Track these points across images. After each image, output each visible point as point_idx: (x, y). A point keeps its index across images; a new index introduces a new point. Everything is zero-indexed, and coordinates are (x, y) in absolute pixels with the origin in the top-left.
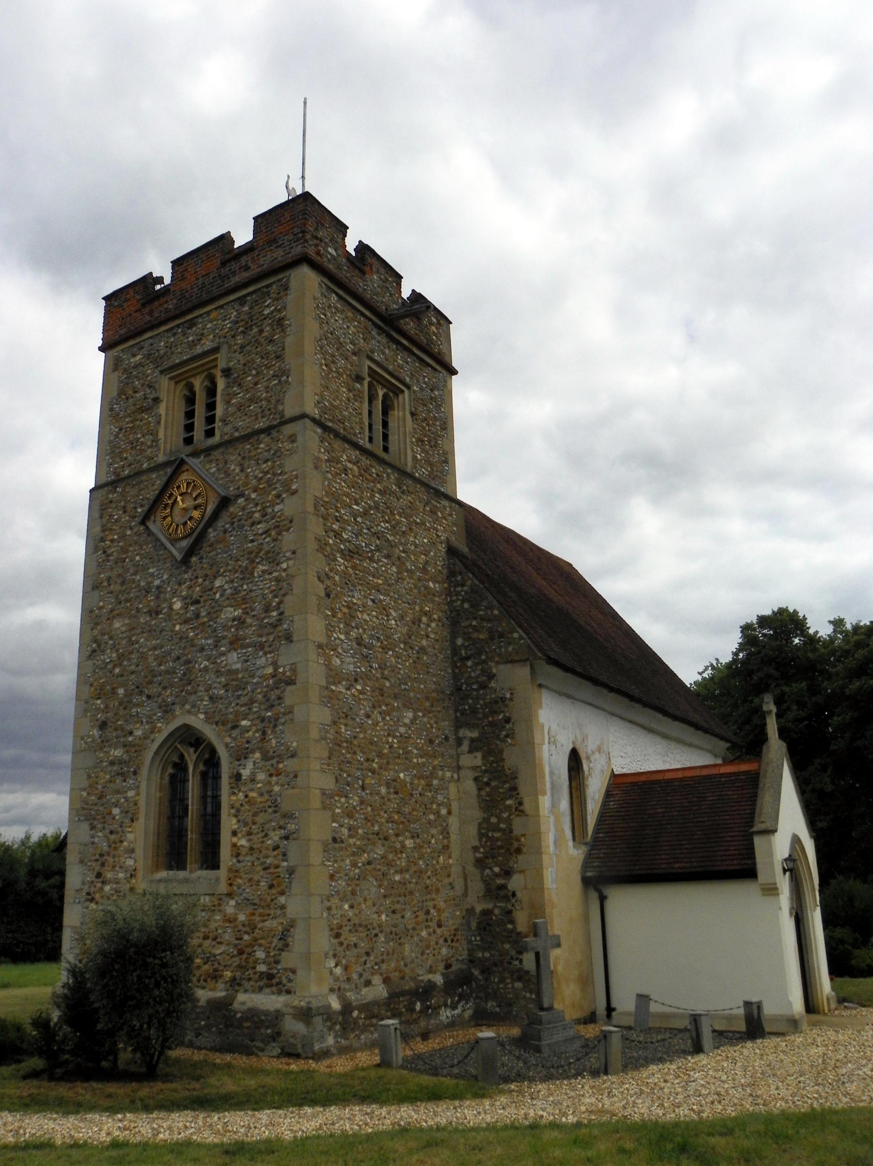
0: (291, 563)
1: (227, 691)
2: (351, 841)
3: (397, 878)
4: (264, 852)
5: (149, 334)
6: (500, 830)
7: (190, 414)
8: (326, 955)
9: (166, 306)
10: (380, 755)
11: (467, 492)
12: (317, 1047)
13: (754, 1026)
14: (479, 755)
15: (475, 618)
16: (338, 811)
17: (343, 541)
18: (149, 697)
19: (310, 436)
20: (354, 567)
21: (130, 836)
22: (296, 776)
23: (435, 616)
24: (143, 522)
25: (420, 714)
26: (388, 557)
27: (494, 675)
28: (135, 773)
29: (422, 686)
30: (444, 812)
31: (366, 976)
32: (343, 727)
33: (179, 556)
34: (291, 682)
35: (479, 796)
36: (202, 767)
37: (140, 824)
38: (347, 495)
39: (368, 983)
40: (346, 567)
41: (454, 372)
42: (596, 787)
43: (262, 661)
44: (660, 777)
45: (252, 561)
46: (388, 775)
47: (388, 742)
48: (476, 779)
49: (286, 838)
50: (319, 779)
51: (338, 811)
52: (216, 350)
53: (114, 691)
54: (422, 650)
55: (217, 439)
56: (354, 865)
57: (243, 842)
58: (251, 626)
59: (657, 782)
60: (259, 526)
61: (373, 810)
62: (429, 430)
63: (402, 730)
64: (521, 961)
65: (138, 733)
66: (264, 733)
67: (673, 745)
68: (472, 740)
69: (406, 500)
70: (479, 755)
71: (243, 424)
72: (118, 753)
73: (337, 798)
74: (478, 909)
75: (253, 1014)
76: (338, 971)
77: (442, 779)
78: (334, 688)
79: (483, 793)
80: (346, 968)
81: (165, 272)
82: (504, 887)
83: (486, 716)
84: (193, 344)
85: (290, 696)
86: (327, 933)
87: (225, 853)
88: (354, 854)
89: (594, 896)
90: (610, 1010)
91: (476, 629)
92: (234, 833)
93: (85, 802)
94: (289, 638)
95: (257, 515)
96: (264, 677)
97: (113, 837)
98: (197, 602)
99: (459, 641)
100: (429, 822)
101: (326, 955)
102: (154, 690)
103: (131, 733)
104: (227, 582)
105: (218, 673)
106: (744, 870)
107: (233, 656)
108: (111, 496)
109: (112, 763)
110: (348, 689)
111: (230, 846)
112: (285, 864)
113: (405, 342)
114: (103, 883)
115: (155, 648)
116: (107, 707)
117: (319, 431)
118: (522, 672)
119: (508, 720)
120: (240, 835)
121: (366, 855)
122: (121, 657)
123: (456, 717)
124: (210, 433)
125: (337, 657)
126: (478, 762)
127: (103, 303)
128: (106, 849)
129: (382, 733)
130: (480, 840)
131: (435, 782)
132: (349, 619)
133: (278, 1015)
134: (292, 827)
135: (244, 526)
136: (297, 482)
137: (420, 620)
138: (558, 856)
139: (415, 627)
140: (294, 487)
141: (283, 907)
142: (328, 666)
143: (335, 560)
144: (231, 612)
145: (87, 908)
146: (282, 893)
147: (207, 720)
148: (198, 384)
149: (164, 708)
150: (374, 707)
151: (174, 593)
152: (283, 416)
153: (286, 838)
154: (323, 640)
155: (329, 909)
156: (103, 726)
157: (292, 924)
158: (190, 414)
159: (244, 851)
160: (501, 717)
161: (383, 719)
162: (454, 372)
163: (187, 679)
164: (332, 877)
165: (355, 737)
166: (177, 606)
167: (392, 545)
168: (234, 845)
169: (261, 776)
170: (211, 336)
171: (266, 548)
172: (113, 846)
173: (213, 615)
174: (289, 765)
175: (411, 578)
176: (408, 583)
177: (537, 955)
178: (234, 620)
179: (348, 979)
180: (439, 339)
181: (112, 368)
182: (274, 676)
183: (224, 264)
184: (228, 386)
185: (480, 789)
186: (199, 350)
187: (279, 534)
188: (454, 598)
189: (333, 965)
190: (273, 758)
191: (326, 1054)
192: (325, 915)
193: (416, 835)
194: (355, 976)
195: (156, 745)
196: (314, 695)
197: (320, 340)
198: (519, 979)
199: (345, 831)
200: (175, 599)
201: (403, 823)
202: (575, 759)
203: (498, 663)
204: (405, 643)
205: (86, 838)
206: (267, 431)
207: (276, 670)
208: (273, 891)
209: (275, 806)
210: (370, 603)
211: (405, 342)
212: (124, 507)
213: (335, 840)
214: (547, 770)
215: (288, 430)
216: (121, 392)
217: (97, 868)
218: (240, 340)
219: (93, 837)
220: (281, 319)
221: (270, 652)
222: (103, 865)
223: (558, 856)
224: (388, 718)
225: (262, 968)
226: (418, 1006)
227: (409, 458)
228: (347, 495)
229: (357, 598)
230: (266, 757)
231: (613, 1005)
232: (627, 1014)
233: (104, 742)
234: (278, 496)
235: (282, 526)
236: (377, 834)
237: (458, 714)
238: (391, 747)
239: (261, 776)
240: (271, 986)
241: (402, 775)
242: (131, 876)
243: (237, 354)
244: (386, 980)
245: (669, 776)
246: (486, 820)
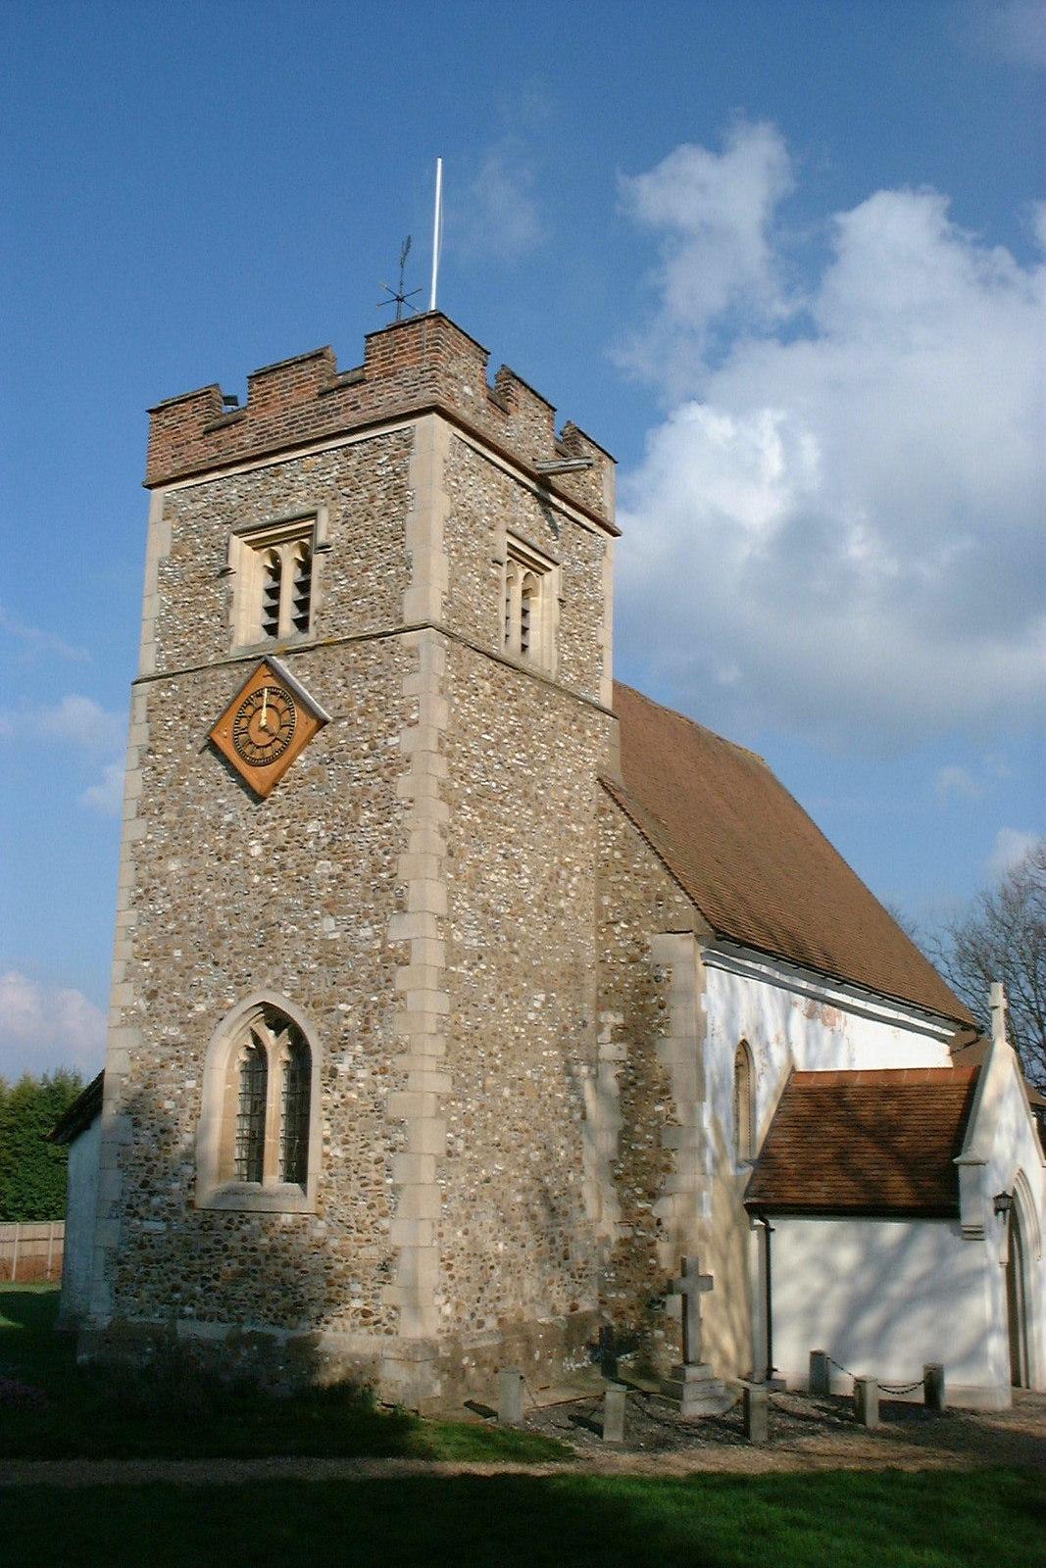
0: (408, 813)
1: (320, 964)
2: (468, 1155)
4: (364, 1165)
5: (217, 475)
7: (274, 593)
9: (240, 439)
10: (505, 1048)
14: (624, 1046)
16: (454, 1118)
17: (470, 783)
19: (434, 656)
20: (482, 815)
22: (406, 1077)
23: (577, 869)
25: (554, 995)
27: (648, 948)
29: (558, 959)
32: (462, 1016)
35: (621, 1097)
40: (473, 816)
42: (766, 1092)
45: (356, 805)
46: (511, 1073)
47: (513, 1032)
50: (432, 1082)
51: (454, 1118)
56: (471, 1183)
57: (338, 1152)
60: (367, 761)
61: (494, 1116)
62: (581, 618)
63: (532, 1016)
65: (201, 1008)
71: (351, 624)
72: (173, 1031)
73: (453, 1104)
76: (448, 1310)
78: (453, 969)
79: (627, 1094)
80: (457, 1306)
84: (277, 501)
85: (402, 979)
86: (437, 1263)
88: (470, 1170)
92: (326, 1141)
94: (401, 907)
95: (365, 747)
99: (606, 901)
104: (323, 828)
108: (163, 694)
109: (164, 1044)
110: (470, 969)
111: (320, 1156)
112: (390, 1181)
114: (151, 1194)
115: (225, 902)
116: (157, 971)
120: (333, 1144)
121: (483, 1171)
123: (598, 997)
124: (302, 624)
125: (459, 930)
126: (624, 1055)
128: (155, 1151)
129: (507, 1021)
130: (620, 1152)
132: (476, 882)
134: (400, 1137)
135: (346, 758)
136: (418, 711)
137: (558, 874)
138: (705, 1199)
139: (552, 885)
140: (413, 717)
142: (449, 943)
144: (324, 867)
145: (128, 1224)
146: (384, 1215)
147: (295, 998)
149: (236, 980)
150: (500, 989)
152: (401, 621)
153: (392, 1150)
154: (443, 911)
156: (152, 995)
158: (274, 593)
160: (654, 1001)
161: (510, 1003)
164: (444, 1198)
165: (477, 1028)
167: (530, 780)
168: (326, 1155)
170: (304, 493)
171: (375, 789)
174: (400, 1062)
175: (549, 820)
176: (546, 827)
177: (685, 1296)
178: (331, 877)
180: (598, 489)
186: (286, 512)
187: (393, 774)
188: (603, 844)
190: (378, 1052)
192: (435, 1243)
193: (542, 1146)
194: (467, 1317)
196: (432, 981)
197: (451, 518)
199: (460, 1144)
200: (253, 842)
201: (527, 1131)
204: (539, 907)
208: (375, 1212)
210: (500, 859)
213: (449, 1154)
215: (407, 638)
216: (175, 550)
217: (143, 1175)
221: (377, 923)
222: (150, 1171)
223: (705, 1199)
224: (515, 1003)
233: (154, 1015)
234: (391, 726)
235: (397, 765)
236: (498, 1145)
237: (601, 994)
238: (517, 1038)
240: (366, 1325)
241: (529, 1073)
242: (190, 1186)
243: (339, 523)
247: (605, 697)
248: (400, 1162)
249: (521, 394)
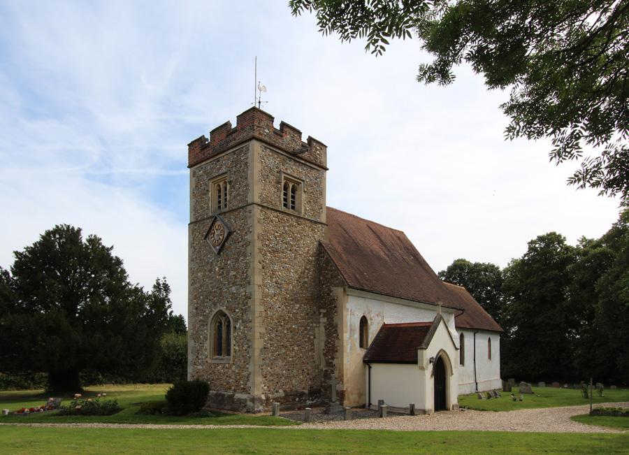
3: (291, 359)
5: (204, 163)
7: (220, 197)
8: (261, 383)
12: (256, 409)
13: (412, 411)
14: (326, 318)
19: (257, 212)
24: (205, 239)
26: (290, 250)
30: (312, 337)
31: (276, 389)
33: (216, 253)
34: (250, 298)
37: (208, 341)
38: (272, 230)
39: (277, 392)
41: (327, 169)
43: (242, 290)
44: (398, 326)
48: (325, 327)
52: (226, 173)
53: (199, 298)
54: (306, 282)
55: (227, 209)
57: (237, 348)
59: (397, 328)
65: (207, 312)
67: (423, 311)
68: (324, 313)
69: (299, 228)
70: (326, 318)
74: (324, 369)
75: (239, 400)
76: (266, 387)
77: (312, 327)
80: (268, 387)
81: (208, 136)
82: (331, 363)
83: (329, 305)
85: (250, 302)
87: (232, 351)
89: (367, 367)
90: (370, 404)
91: (327, 274)
94: (249, 283)
96: (242, 296)
98: (223, 269)
100: (305, 341)
101: (261, 383)
102: (211, 297)
105: (230, 294)
106: (414, 361)
107: (234, 288)
113: (303, 162)
115: (211, 284)
117: (260, 208)
118: (340, 290)
119: (335, 307)
122: (201, 286)
126: (326, 321)
127: (188, 147)
131: (309, 328)
133: (246, 400)
137: (304, 271)
138: (351, 355)
141: (248, 368)
143: (266, 255)
144: (233, 273)
147: (227, 308)
148: (221, 184)
151: (216, 265)
155: (262, 369)
156: (196, 309)
157: (250, 373)
158: (220, 197)
162: (327, 169)
163: (221, 295)
166: (217, 269)
169: (242, 328)
171: (243, 251)
172: (201, 348)
173: (228, 272)
179: (269, 391)
181: (193, 175)
182: (245, 295)
183: (227, 136)
184: (231, 188)
186: (221, 172)
189: (263, 386)
191: (259, 411)
195: (212, 316)
199: (269, 345)
202: (364, 321)
205: (193, 345)
209: (246, 337)
211: (303, 162)
213: (265, 348)
214: (349, 324)
215: (249, 208)
216: (196, 186)
218: (234, 169)
220: (247, 163)
223: (351, 355)
225: (242, 386)
226: (297, 399)
227: (303, 209)
228: (272, 230)
229: (276, 267)
230: (243, 322)
231: (371, 403)
232: (375, 406)
235: (248, 244)
239: (242, 328)
244: (285, 391)
245: (403, 326)
246: (327, 340)
247: (323, 219)
248: (250, 350)
249: (288, 130)
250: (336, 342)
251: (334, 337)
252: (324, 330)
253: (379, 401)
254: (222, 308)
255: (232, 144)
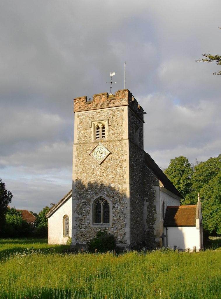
6: (152, 217)
11: (146, 150)
15: (148, 176)
18: (92, 190)
21: (88, 216)
28: (89, 205)
36: (104, 204)
48: (147, 207)
49: (125, 218)
58: (116, 179)
64: (155, 240)
66: (120, 199)
68: (147, 200)
82: (152, 227)
84: (99, 117)
89: (165, 229)
93: (76, 209)
97: (84, 216)
103: (88, 197)
109: (83, 202)
113: (138, 118)
126: (148, 204)
134: (126, 216)
144: (111, 176)
146: (124, 227)
153: (125, 218)
156: (80, 195)
157: (126, 233)
159: (115, 220)
185: (148, 209)
186: (101, 119)
195: (94, 200)
198: (154, 243)
203: (153, 186)
206: (120, 141)
207: (122, 188)
209: (122, 213)
211: (138, 118)
212: (83, 150)
217: (80, 222)
219: (79, 216)
225: (120, 240)
233: (81, 198)
239: (119, 207)
250: (155, 215)
251: (154, 213)
252: (147, 209)
253: (175, 246)
254: (102, 195)
255: (110, 105)
